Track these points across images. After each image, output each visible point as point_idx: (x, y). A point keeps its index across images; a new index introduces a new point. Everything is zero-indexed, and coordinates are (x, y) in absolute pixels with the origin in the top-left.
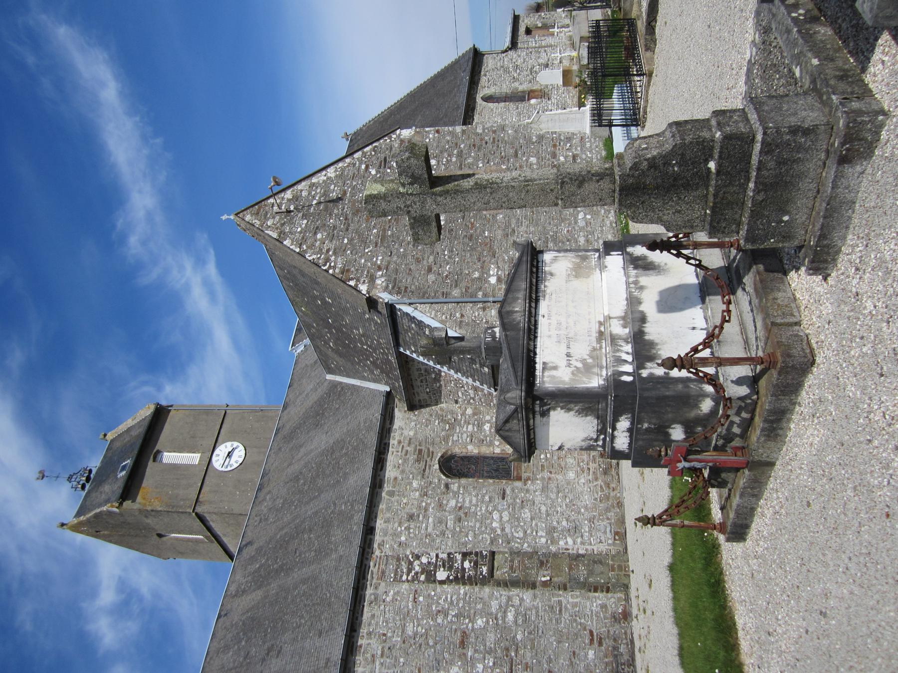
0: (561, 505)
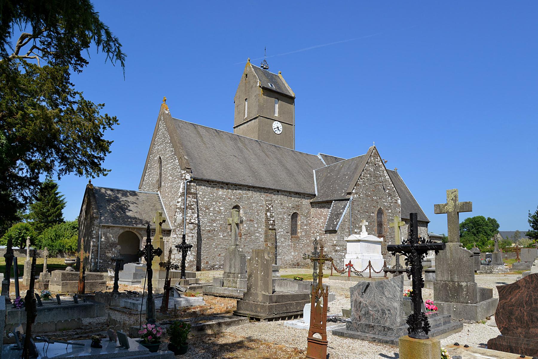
0: (284, 250)
